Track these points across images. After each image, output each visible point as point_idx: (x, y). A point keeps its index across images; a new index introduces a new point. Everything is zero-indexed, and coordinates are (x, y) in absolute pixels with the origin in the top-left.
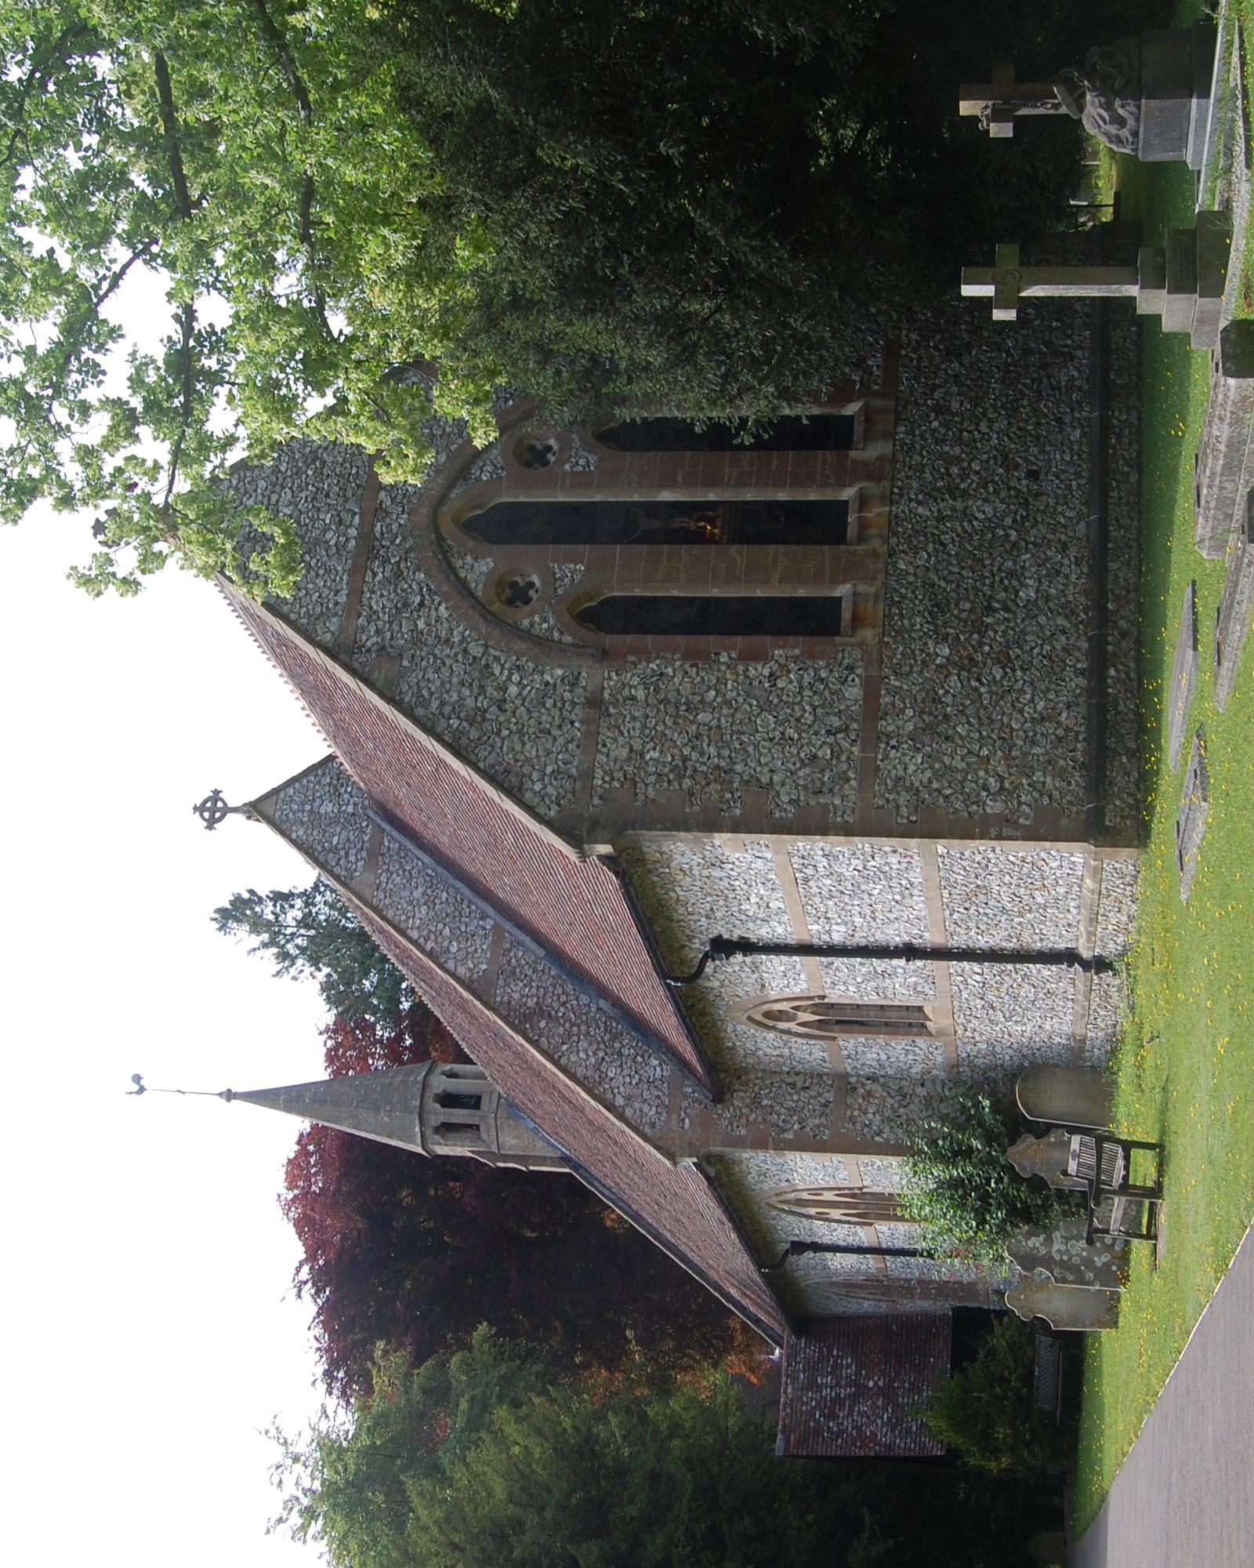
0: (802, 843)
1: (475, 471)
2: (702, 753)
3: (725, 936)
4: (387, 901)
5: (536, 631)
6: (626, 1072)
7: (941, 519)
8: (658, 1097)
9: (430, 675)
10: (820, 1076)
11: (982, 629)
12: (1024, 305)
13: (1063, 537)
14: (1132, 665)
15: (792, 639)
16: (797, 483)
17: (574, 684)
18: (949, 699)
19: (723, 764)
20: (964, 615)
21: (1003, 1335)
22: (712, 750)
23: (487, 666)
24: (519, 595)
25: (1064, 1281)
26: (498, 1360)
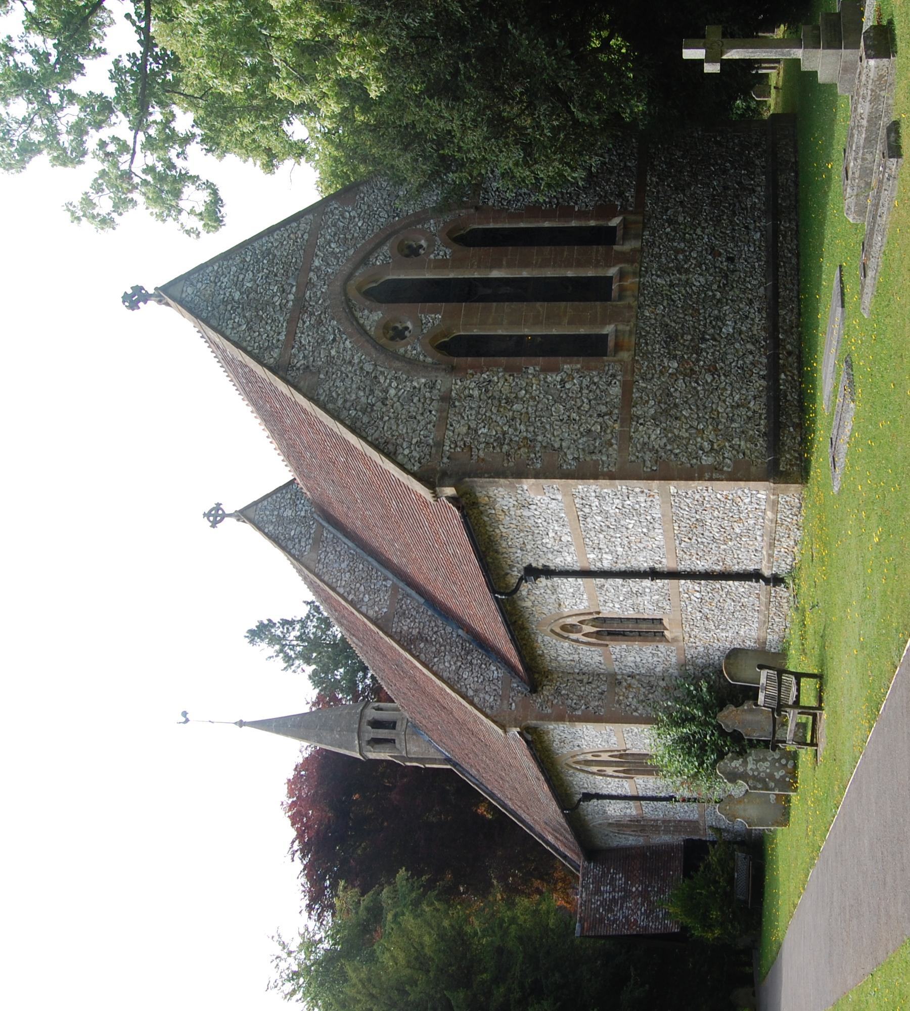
0: (581, 487)
1: (372, 260)
2: (516, 430)
3: (534, 565)
4: (325, 570)
5: (408, 355)
6: (475, 674)
7: (672, 285)
8: (495, 690)
9: (338, 383)
10: (599, 675)
11: (699, 351)
12: (725, 64)
13: (750, 296)
14: (796, 372)
15: (575, 358)
16: (580, 265)
17: (432, 387)
18: (677, 394)
19: (529, 436)
20: (687, 343)
21: (715, 855)
22: (522, 427)
23: (376, 377)
24: (399, 334)
25: (755, 788)
26: (412, 890)
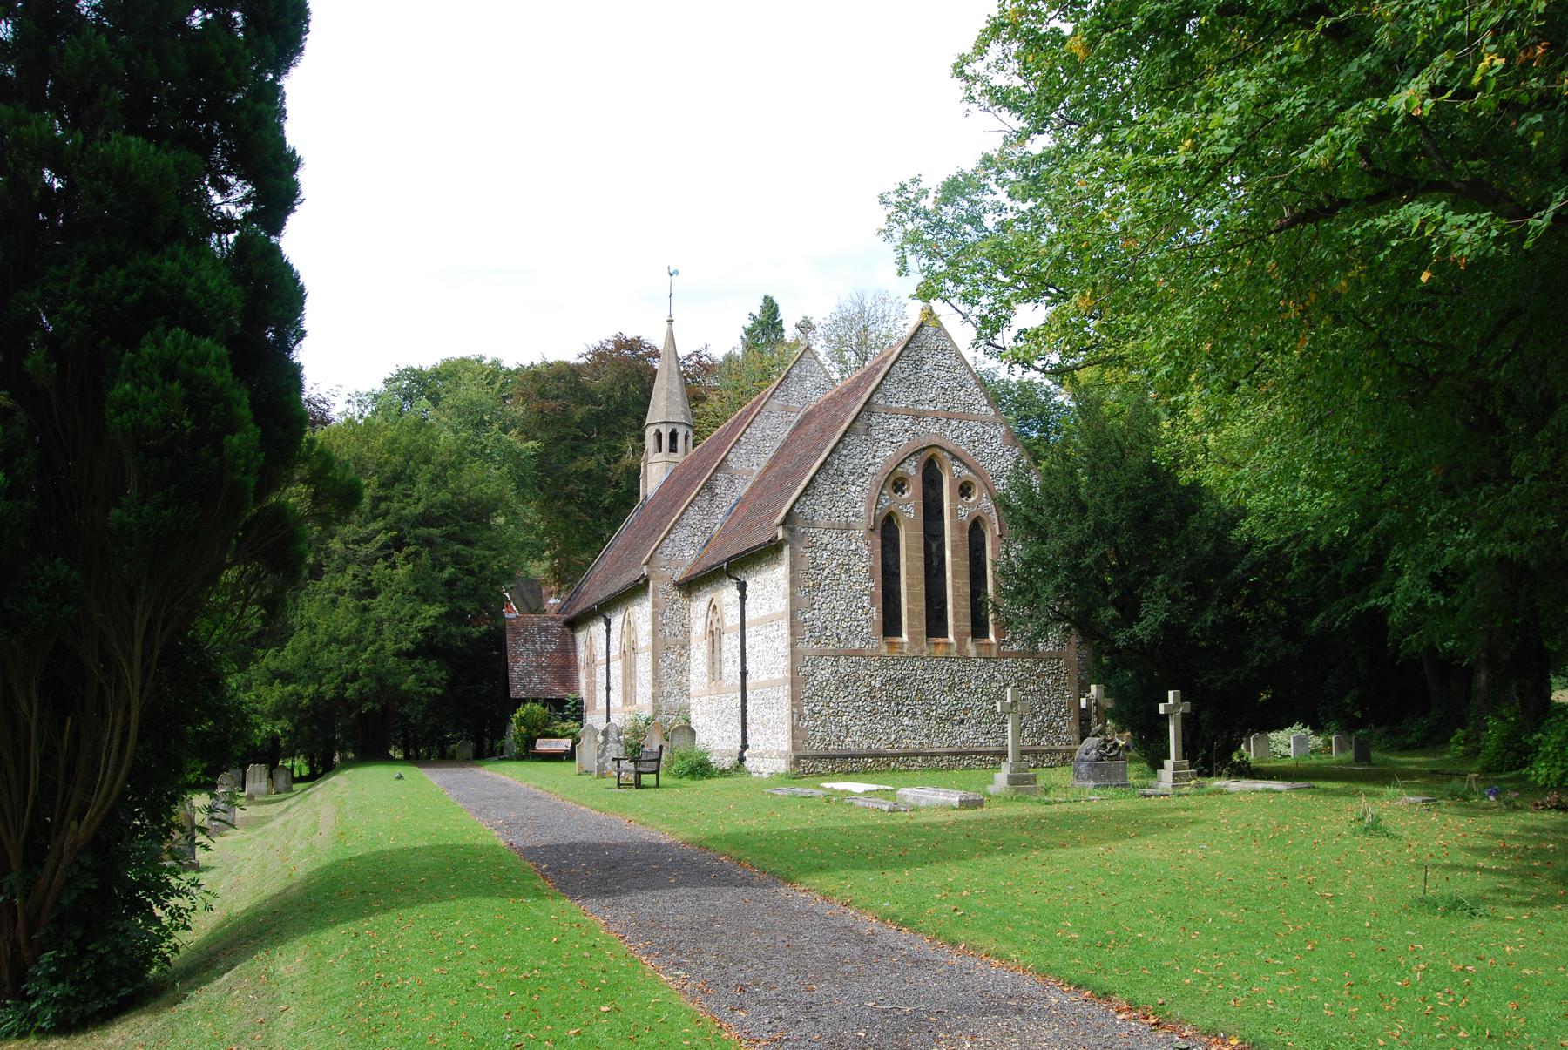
12: (1165, 718)
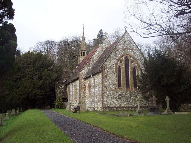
12: (166, 101)
24: (121, 61)
